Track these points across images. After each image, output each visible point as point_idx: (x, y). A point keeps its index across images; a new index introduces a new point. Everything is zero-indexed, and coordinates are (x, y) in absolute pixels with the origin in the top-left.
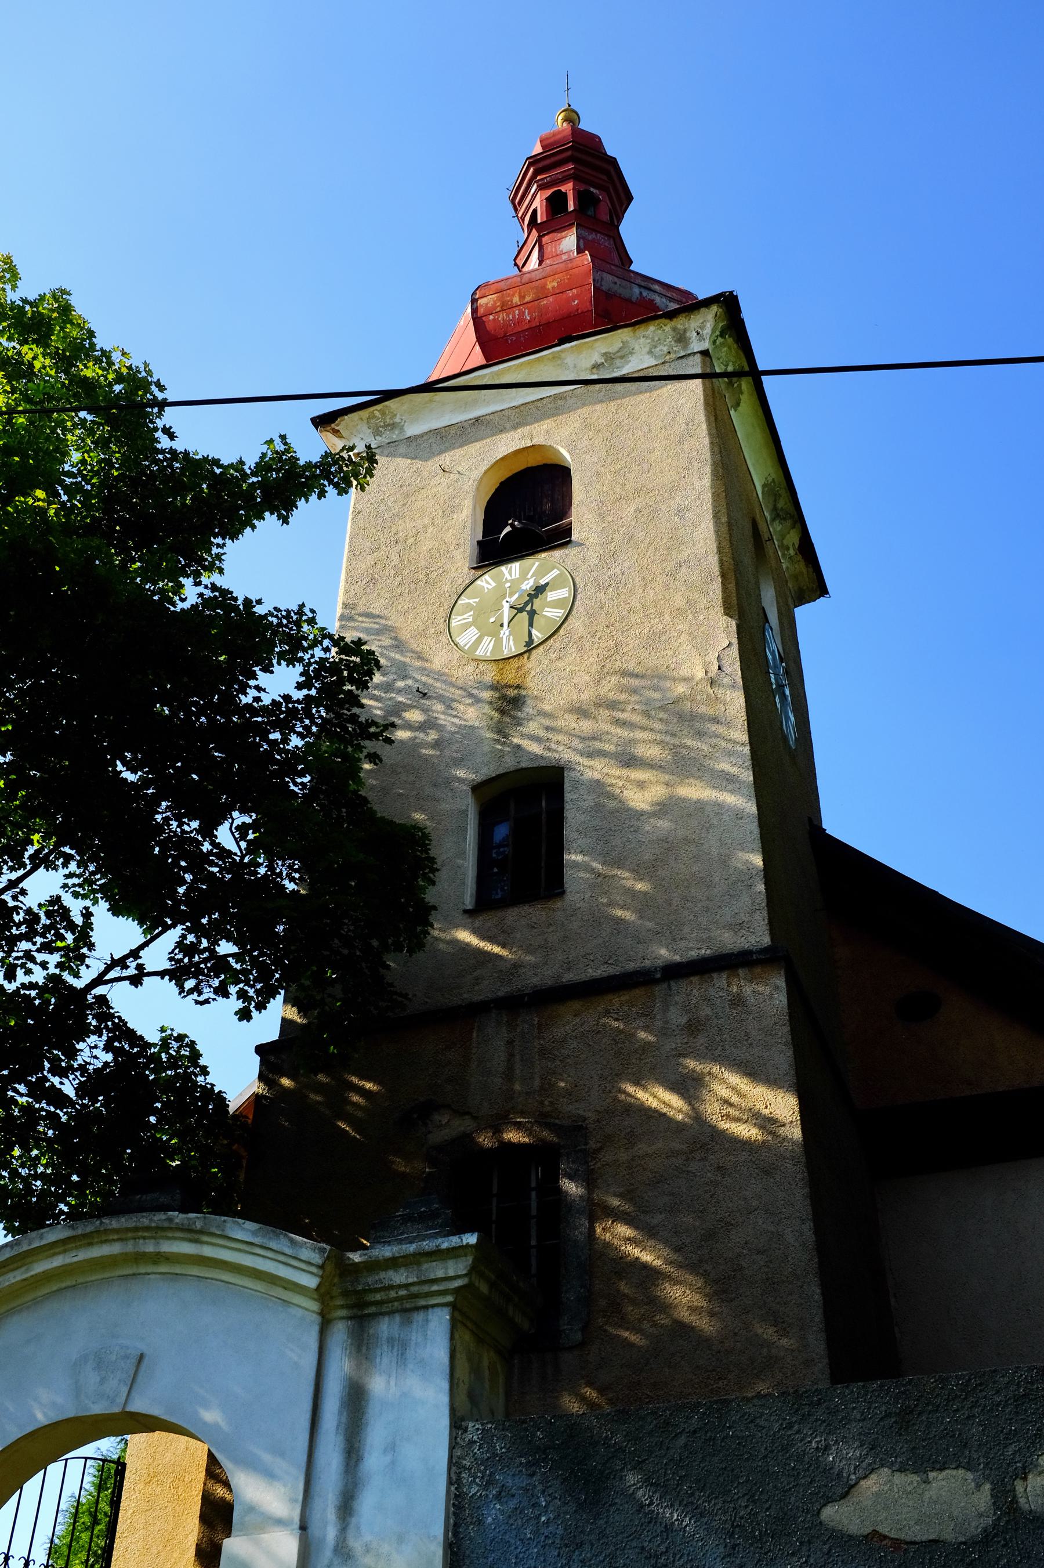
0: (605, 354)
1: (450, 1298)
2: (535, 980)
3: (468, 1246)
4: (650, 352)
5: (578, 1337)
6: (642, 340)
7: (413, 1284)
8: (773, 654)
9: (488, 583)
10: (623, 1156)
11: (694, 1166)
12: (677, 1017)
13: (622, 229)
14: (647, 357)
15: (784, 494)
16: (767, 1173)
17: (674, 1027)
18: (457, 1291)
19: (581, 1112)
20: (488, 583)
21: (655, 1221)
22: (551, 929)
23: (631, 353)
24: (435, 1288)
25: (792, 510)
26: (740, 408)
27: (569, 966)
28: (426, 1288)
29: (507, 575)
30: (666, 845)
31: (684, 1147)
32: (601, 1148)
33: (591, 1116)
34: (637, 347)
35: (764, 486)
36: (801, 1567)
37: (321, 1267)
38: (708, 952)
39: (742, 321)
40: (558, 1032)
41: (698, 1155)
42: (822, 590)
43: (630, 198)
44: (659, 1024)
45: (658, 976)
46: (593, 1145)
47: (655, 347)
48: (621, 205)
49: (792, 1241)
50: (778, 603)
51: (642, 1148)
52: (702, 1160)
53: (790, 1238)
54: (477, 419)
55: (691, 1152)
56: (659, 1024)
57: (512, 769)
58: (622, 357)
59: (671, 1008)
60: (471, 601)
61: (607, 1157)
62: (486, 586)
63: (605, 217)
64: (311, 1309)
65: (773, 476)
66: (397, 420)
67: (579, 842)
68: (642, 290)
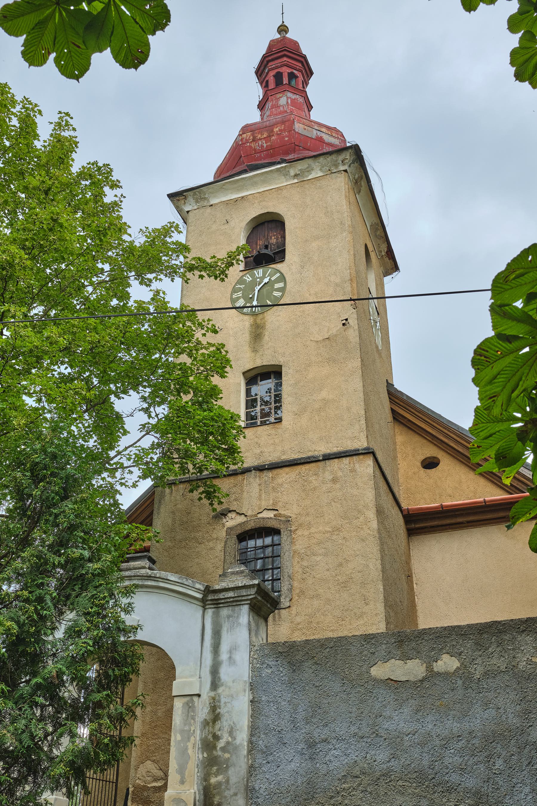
0: (301, 169)
1: (249, 602)
2: (270, 459)
3: (255, 584)
4: (321, 170)
5: (288, 604)
6: (317, 164)
7: (236, 597)
8: (373, 309)
9: (248, 278)
10: (306, 533)
11: (334, 537)
12: (328, 476)
13: (308, 89)
14: (319, 172)
15: (380, 227)
16: (363, 540)
17: (327, 480)
18: (251, 599)
19: (289, 515)
20: (248, 278)
21: (318, 559)
22: (277, 436)
23: (312, 170)
24: (244, 598)
25: (383, 235)
26: (361, 193)
27: (284, 452)
28: (240, 598)
29: (257, 275)
30: (324, 402)
31: (330, 530)
32: (296, 530)
33: (293, 516)
34: (315, 167)
35: (371, 226)
36: (1, 383)
37: (204, 591)
38: (342, 448)
39: (362, 156)
40: (280, 481)
41: (336, 533)
42: (396, 268)
43: (312, 73)
44: (321, 479)
45: (321, 458)
46: (293, 528)
47: (323, 167)
48: (308, 77)
49: (372, 568)
50: (376, 280)
51: (313, 530)
52: (337, 535)
53: (371, 567)
54: (243, 197)
55: (333, 531)
56: (321, 479)
57: (260, 365)
58: (308, 171)
59: (326, 472)
60: (241, 286)
61: (299, 532)
62: (248, 279)
63: (301, 87)
64: (265, 630)
65: (375, 221)
66: (206, 196)
67: (288, 399)
68: (318, 132)
